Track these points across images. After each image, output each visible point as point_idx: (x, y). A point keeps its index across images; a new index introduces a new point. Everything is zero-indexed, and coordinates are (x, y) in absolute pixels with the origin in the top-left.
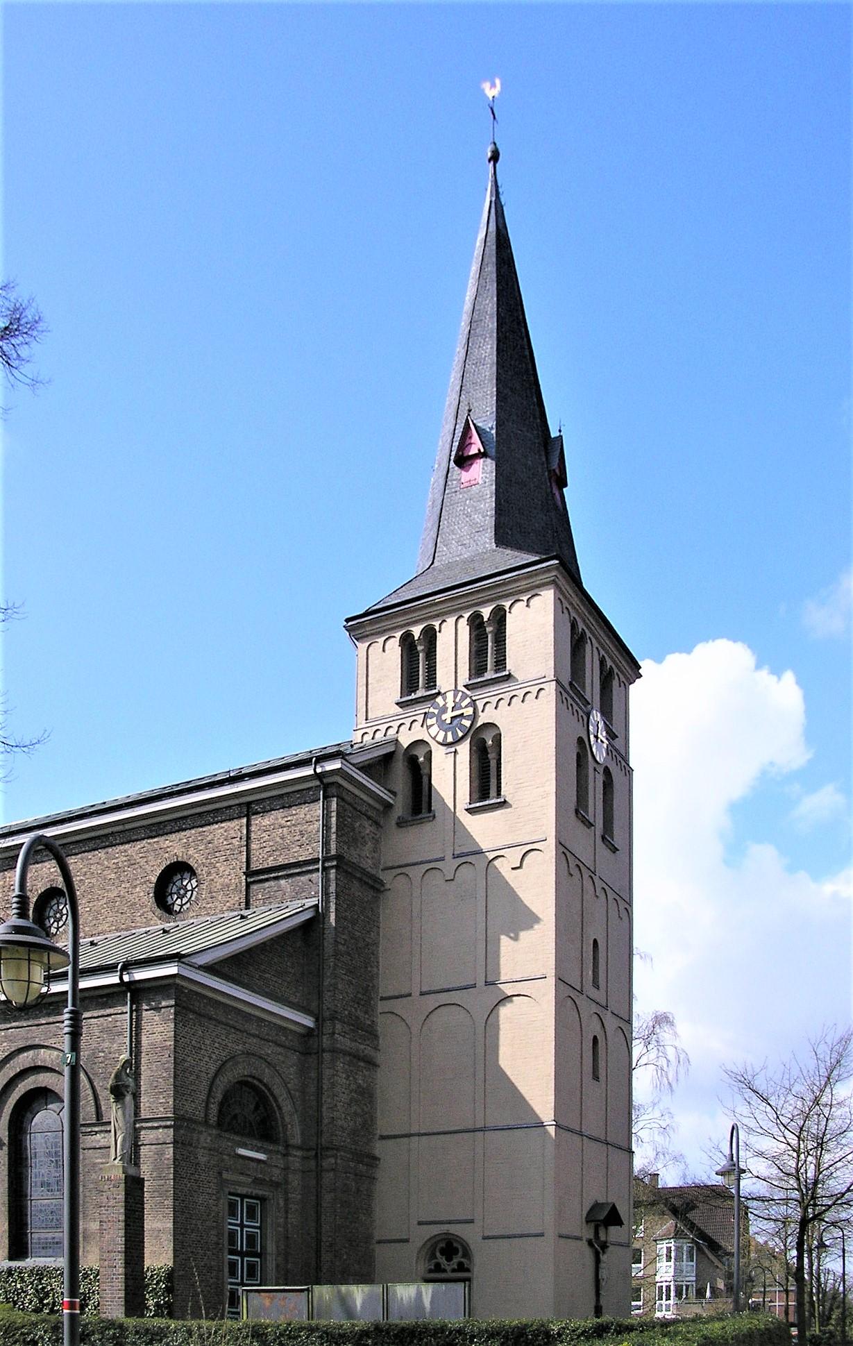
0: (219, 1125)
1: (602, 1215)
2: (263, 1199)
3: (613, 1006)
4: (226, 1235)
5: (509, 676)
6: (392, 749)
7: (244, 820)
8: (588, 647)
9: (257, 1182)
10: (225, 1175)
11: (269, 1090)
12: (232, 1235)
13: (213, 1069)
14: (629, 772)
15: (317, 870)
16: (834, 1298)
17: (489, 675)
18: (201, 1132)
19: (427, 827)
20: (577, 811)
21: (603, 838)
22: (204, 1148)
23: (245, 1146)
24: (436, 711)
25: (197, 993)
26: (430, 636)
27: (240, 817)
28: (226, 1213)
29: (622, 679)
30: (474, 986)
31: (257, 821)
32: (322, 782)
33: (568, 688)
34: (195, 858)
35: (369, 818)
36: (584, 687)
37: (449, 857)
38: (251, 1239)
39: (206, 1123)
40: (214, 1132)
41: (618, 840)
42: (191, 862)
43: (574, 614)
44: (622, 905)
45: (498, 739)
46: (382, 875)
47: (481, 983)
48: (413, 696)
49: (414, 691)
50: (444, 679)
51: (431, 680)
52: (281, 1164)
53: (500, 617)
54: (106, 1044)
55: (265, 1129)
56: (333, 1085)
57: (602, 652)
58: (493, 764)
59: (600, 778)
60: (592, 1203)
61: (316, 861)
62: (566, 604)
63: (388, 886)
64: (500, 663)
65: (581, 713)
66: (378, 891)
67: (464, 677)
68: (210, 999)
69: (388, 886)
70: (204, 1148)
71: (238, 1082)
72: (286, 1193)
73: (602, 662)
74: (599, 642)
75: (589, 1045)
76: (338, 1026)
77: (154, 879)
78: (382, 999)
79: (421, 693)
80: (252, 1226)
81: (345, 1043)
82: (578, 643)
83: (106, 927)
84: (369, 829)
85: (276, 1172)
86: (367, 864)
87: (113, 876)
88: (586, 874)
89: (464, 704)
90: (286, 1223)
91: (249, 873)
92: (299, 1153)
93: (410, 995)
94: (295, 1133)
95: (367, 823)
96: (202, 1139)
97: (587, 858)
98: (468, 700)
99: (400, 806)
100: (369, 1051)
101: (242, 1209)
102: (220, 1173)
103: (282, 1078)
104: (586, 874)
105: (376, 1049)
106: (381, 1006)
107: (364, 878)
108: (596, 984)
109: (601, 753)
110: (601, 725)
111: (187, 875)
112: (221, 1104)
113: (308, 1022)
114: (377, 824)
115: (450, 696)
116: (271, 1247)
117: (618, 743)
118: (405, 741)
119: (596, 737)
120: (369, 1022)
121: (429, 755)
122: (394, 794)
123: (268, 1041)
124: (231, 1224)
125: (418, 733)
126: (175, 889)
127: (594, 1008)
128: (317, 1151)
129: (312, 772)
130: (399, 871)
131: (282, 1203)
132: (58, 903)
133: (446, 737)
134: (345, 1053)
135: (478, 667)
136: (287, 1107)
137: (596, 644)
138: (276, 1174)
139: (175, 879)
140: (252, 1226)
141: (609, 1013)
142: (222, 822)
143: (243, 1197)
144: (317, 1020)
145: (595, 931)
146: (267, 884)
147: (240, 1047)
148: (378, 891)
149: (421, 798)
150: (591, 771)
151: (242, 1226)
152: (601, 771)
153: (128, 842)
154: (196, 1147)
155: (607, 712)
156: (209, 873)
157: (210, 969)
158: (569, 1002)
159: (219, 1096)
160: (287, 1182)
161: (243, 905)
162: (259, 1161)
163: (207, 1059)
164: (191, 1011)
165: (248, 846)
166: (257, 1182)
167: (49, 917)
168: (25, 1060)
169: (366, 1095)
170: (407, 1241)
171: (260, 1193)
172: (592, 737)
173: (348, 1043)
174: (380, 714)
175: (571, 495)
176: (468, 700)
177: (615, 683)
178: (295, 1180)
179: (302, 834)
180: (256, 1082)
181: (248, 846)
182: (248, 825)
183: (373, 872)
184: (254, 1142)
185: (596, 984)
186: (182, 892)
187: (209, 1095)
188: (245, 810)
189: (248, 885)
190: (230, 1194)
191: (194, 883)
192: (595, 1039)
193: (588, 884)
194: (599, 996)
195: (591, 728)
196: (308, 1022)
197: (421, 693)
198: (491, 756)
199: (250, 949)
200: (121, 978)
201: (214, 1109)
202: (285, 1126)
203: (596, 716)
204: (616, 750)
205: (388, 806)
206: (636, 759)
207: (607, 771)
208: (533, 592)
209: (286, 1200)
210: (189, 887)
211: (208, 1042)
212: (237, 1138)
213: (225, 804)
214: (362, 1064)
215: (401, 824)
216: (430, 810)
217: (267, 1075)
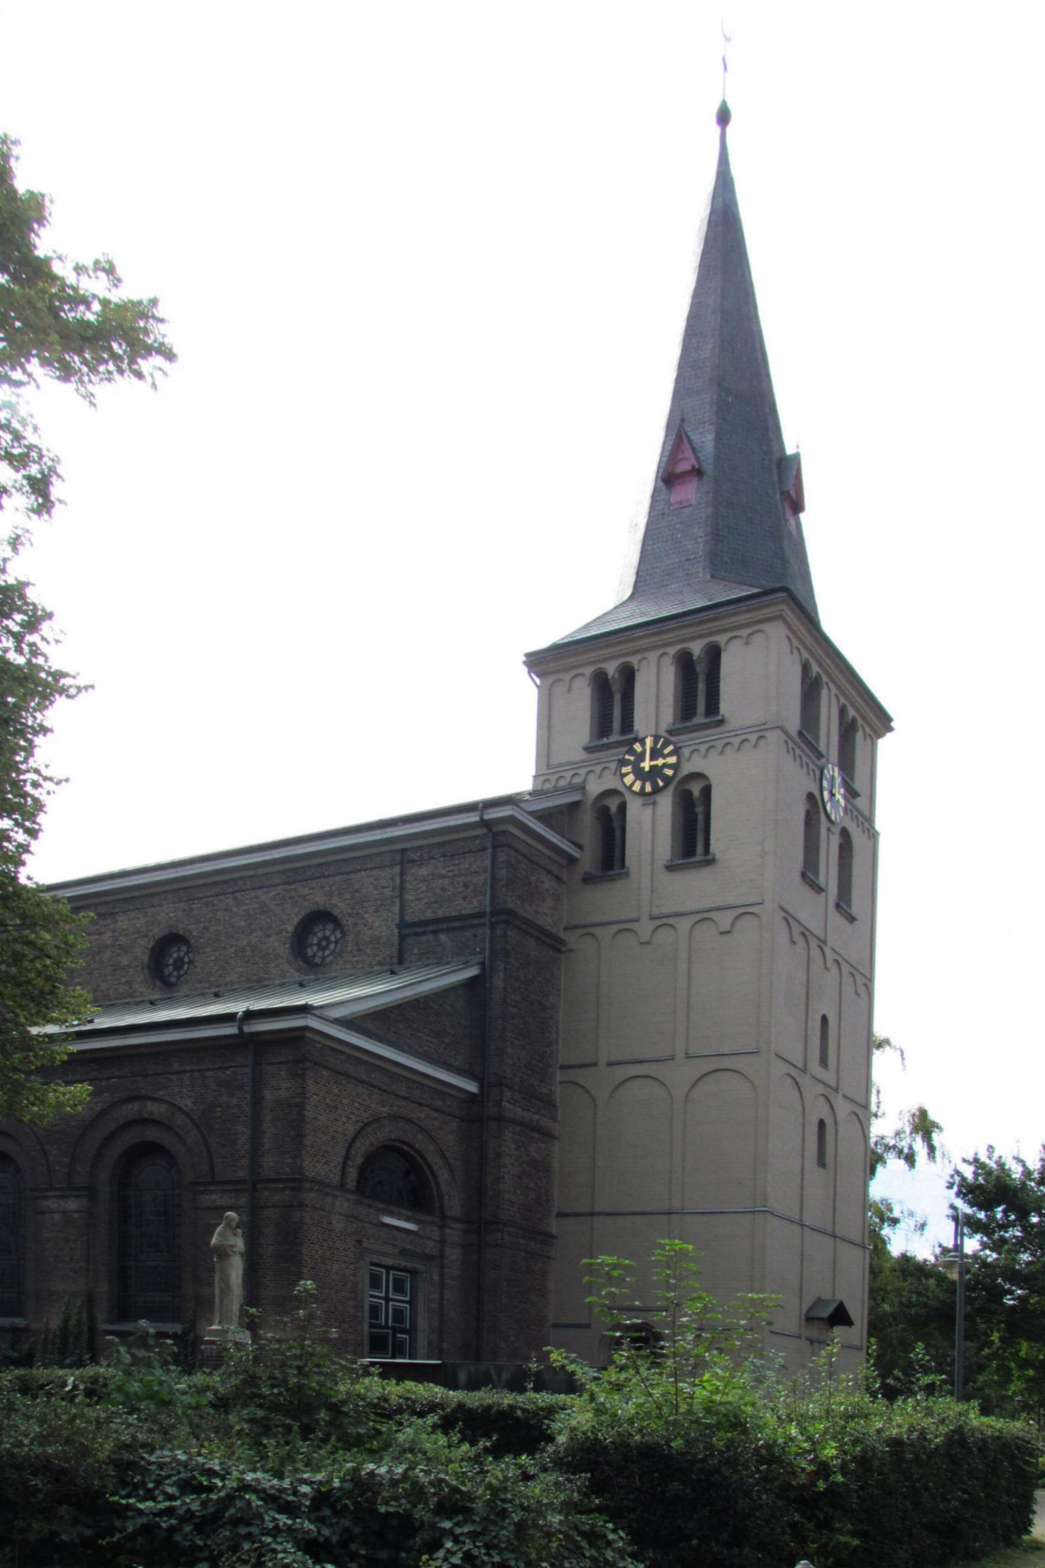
0: (360, 1189)
1: (827, 1312)
2: (413, 1272)
3: (845, 1088)
4: (367, 1308)
5: (722, 722)
6: (576, 797)
7: (397, 869)
8: (824, 693)
9: (404, 1253)
10: (366, 1244)
11: (422, 1157)
12: (374, 1310)
13: (351, 1130)
14: (873, 836)
15: (484, 924)
16: (46, 1340)
17: (699, 719)
18: (335, 1197)
19: (619, 885)
20: (804, 875)
21: (838, 906)
22: (341, 1214)
23: (390, 1214)
24: (632, 758)
25: (332, 1049)
26: (628, 675)
27: (392, 866)
28: (367, 1282)
29: (868, 730)
30: (673, 1058)
31: (414, 871)
32: (490, 830)
33: (798, 740)
34: (340, 906)
35: (549, 872)
36: (817, 738)
37: (645, 918)
38: (399, 1314)
39: (342, 1186)
40: (353, 1197)
41: (856, 908)
42: (335, 912)
43: (805, 655)
44: (860, 980)
45: (707, 792)
46: (562, 934)
47: (680, 1054)
48: (605, 741)
49: (607, 736)
50: (643, 721)
51: (627, 724)
52: (436, 1235)
53: (714, 654)
54: (225, 1098)
55: (417, 1196)
56: (498, 1156)
57: (843, 700)
58: (701, 818)
59: (835, 841)
60: (814, 1299)
61: (482, 915)
62: (796, 643)
63: (569, 947)
64: (713, 706)
65: (812, 766)
66: (560, 951)
67: (668, 715)
68: (349, 1056)
69: (569, 947)
70: (341, 1214)
71: (384, 1147)
72: (442, 1267)
73: (842, 711)
74: (838, 687)
75: (812, 1130)
76: (507, 1094)
77: (290, 928)
78: (563, 1067)
79: (614, 738)
80: (400, 1301)
81: (518, 1112)
82: (811, 689)
83: (235, 977)
84: (548, 883)
85: (431, 1243)
86: (546, 922)
87: (243, 924)
88: (814, 944)
89: (666, 751)
90: (441, 1299)
91: (403, 925)
92: (458, 1226)
93: (595, 1064)
94: (454, 1204)
95: (546, 878)
96: (338, 1203)
97: (815, 926)
98: (671, 748)
99: (588, 859)
100: (544, 1122)
101: (387, 1279)
102: (360, 1242)
103: (442, 1148)
104: (814, 944)
105: (555, 1120)
106: (559, 1076)
107: (542, 937)
108: (824, 1061)
109: (837, 812)
110: (838, 780)
111: (330, 926)
112: (362, 1170)
113: (472, 1087)
114: (558, 878)
115: (649, 742)
116: (422, 1323)
117: (860, 802)
118: (595, 788)
119: (832, 795)
120: (545, 1091)
121: (623, 807)
122: (580, 847)
123: (421, 1105)
124: (371, 1296)
125: (609, 782)
126: (315, 941)
127: (821, 1089)
128: (480, 1223)
129: (477, 819)
130: (585, 930)
131: (436, 1277)
132: (179, 950)
133: (643, 788)
134: (514, 1122)
135: (686, 709)
136: (444, 1177)
137: (834, 690)
138: (430, 1247)
139: (316, 929)
140: (400, 1301)
141: (840, 1097)
142: (371, 869)
143: (388, 1268)
144: (481, 1086)
145: (824, 1006)
146: (424, 938)
147: (386, 1109)
148: (560, 951)
149: (612, 856)
150: (823, 831)
151: (387, 1299)
152: (837, 830)
153: (261, 888)
154: (331, 1212)
155: (847, 764)
156: (356, 924)
157: (348, 1023)
158: (789, 1080)
159: (359, 1160)
160: (442, 1256)
161: (395, 960)
162: (409, 1232)
163: (344, 1119)
164: (325, 1067)
165: (401, 896)
166: (404, 1253)
167: (168, 965)
168: (130, 1110)
169: (540, 1168)
170: (588, 1326)
171: (410, 1265)
172: (826, 795)
173: (519, 1112)
174: (563, 759)
175: (808, 520)
176: (671, 748)
177: (859, 735)
178: (453, 1254)
179: (466, 886)
180: (405, 1147)
181: (401, 896)
182: (402, 874)
183: (554, 930)
184: (403, 1211)
185: (824, 1061)
186: (324, 943)
187: (347, 1157)
188: (398, 858)
189: (402, 938)
190: (372, 1264)
191: (339, 935)
192: (822, 1124)
193: (815, 953)
194: (829, 1076)
195: (825, 784)
196: (472, 1087)
197: (614, 738)
198: (699, 809)
199: (399, 1006)
200: (241, 1029)
201: (353, 1174)
202: (441, 1196)
203: (833, 771)
204: (858, 810)
205: (572, 860)
206: (881, 822)
207: (845, 833)
208: (756, 628)
209: (442, 1275)
210: (333, 938)
211: (345, 1101)
212: (380, 1206)
213: (374, 850)
214: (536, 1135)
215: (587, 880)
216: (623, 865)
217: (419, 1141)
